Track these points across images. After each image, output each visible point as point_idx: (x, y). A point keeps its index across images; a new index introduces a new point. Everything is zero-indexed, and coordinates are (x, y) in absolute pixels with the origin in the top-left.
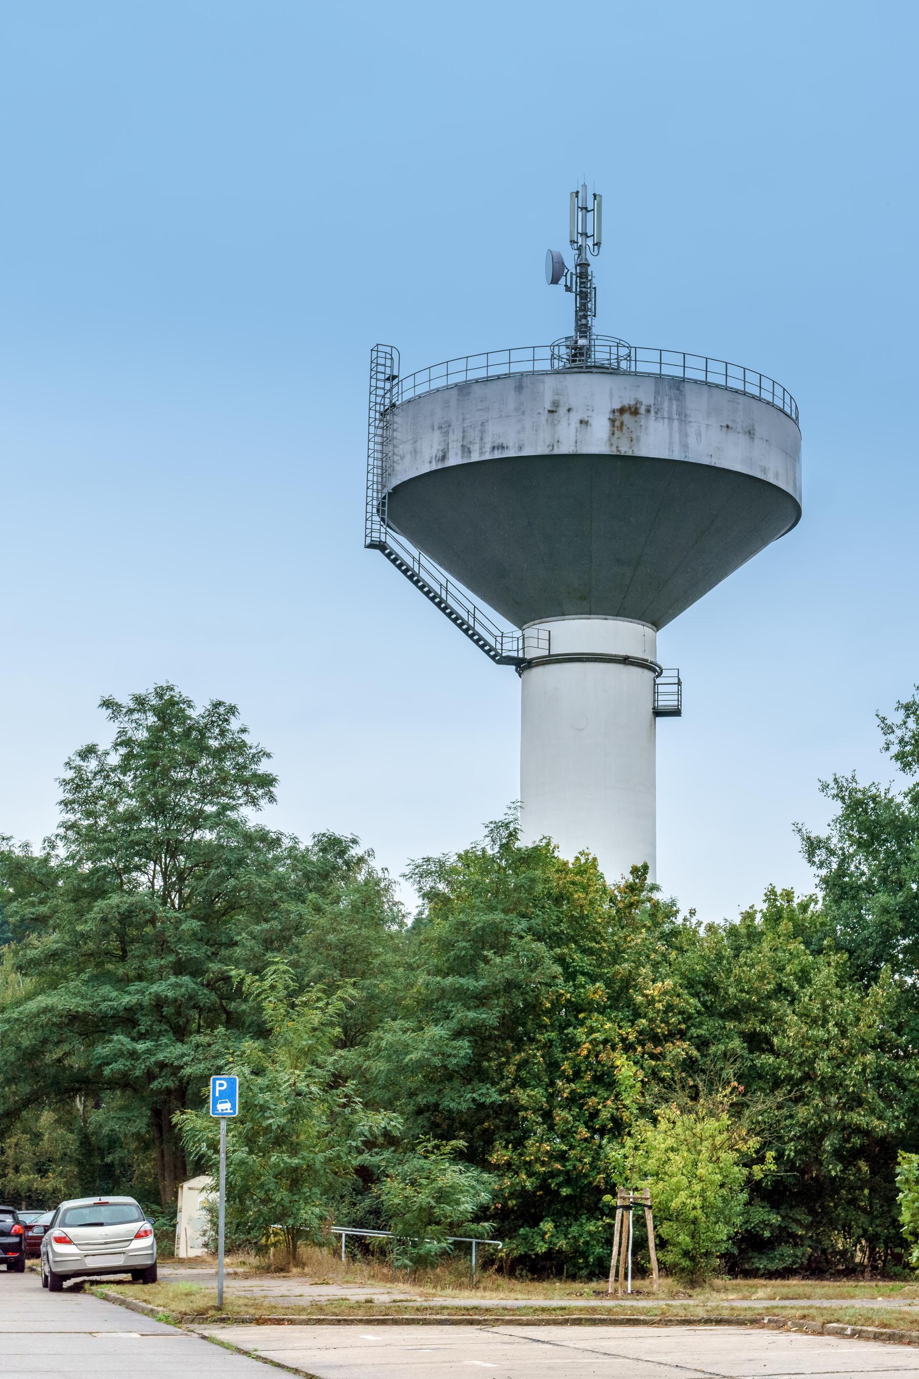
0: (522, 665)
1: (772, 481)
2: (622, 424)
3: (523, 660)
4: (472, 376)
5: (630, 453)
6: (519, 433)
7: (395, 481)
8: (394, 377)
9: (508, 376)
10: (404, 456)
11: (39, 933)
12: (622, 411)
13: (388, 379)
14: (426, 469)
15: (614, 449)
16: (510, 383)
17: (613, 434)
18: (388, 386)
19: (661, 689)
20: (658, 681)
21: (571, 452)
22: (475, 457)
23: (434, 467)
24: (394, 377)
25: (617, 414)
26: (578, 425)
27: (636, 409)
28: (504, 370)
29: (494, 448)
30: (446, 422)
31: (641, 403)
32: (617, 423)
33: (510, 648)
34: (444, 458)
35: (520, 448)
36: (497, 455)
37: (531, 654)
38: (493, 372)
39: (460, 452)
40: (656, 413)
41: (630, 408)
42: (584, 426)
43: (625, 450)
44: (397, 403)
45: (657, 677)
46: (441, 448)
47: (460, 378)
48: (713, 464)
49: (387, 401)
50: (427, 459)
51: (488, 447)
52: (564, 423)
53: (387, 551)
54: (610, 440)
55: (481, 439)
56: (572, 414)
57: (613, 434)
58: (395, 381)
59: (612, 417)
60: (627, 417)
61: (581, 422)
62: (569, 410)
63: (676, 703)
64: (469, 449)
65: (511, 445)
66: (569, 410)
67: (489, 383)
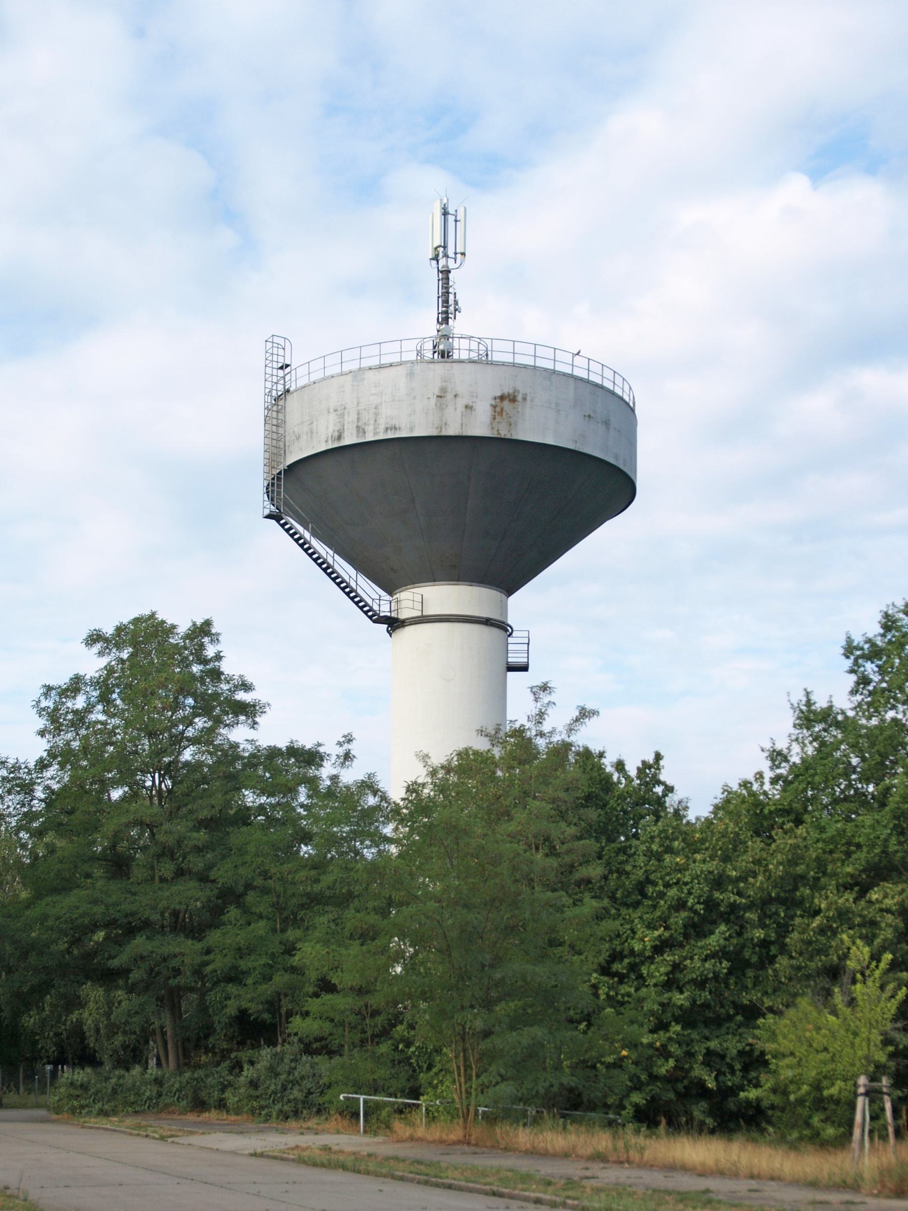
0: (394, 624)
1: (621, 467)
2: (502, 409)
3: (396, 620)
4: (365, 364)
5: (508, 437)
6: (410, 415)
7: (291, 459)
8: (287, 366)
9: (401, 364)
10: (299, 436)
11: (38, 1007)
12: (502, 398)
13: (281, 368)
14: (323, 447)
15: (496, 433)
16: (401, 370)
17: (494, 418)
18: (281, 373)
19: (510, 647)
20: (510, 640)
21: (457, 434)
22: (370, 438)
23: (330, 446)
24: (287, 366)
25: (498, 401)
26: (464, 409)
27: (514, 396)
28: (396, 359)
29: (387, 429)
30: (341, 405)
31: (518, 392)
32: (498, 409)
33: (385, 610)
34: (339, 438)
35: (412, 429)
36: (390, 435)
37: (403, 615)
38: (386, 360)
39: (355, 432)
40: (531, 401)
41: (509, 395)
42: (469, 411)
43: (504, 433)
44: (291, 389)
45: (509, 636)
46: (336, 429)
47: (354, 366)
48: (577, 449)
49: (280, 387)
50: (323, 438)
51: (382, 428)
52: (451, 408)
53: (282, 522)
54: (491, 424)
55: (375, 421)
56: (459, 400)
57: (494, 418)
58: (288, 369)
59: (493, 403)
60: (506, 403)
61: (466, 407)
62: (456, 396)
63: (526, 660)
64: (364, 430)
65: (403, 426)
66: (456, 396)
67: (382, 370)
